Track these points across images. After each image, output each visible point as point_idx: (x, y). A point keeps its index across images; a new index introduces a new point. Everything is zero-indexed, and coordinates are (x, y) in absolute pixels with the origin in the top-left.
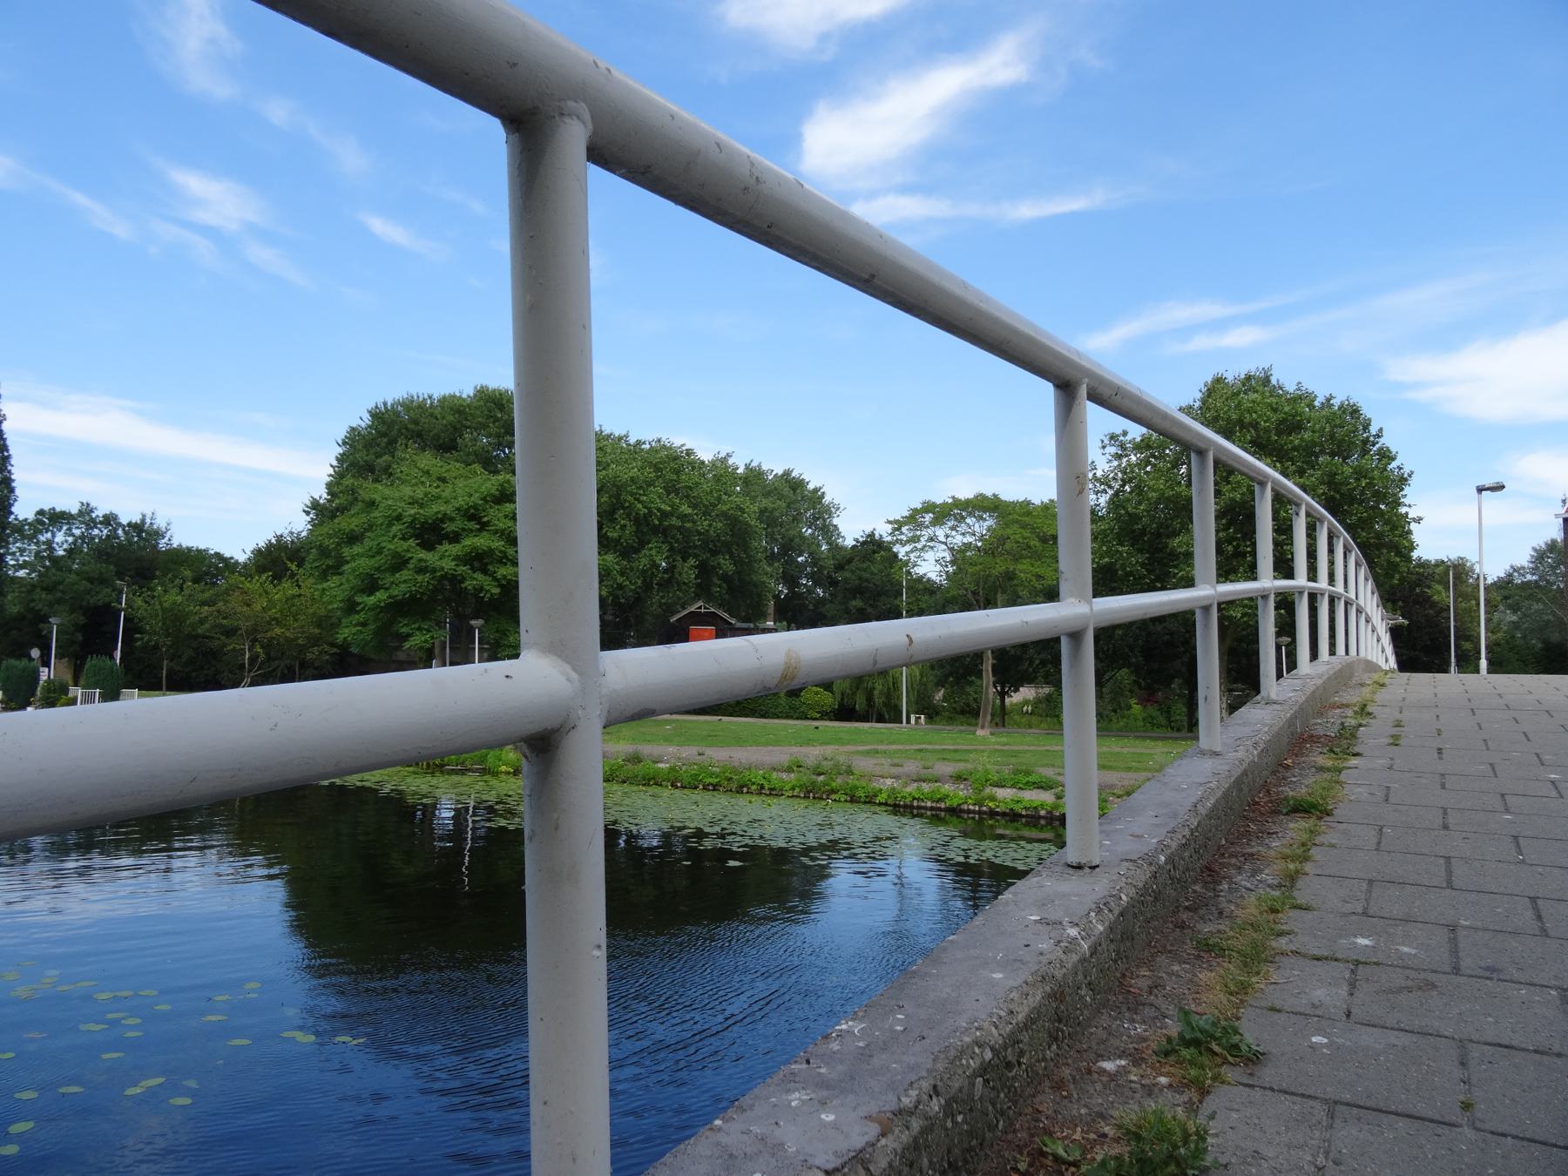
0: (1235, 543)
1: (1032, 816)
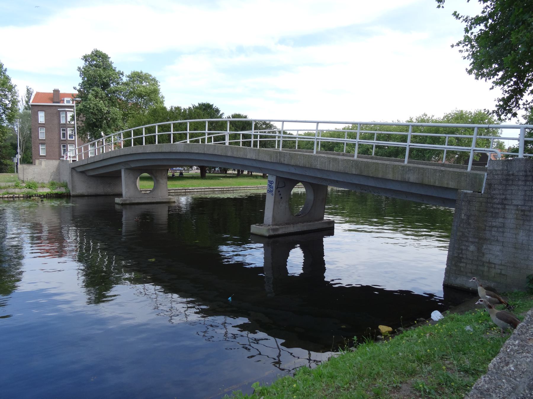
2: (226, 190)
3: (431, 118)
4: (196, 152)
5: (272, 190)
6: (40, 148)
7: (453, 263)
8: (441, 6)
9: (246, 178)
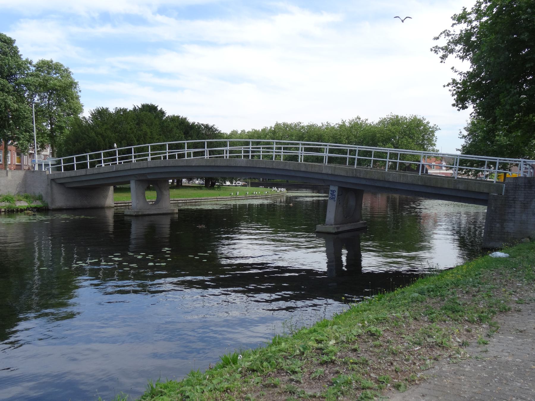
2: (188, 202)
3: (365, 122)
4: (262, 167)
5: (334, 197)
7: (487, 235)
8: (443, 62)
9: (189, 189)
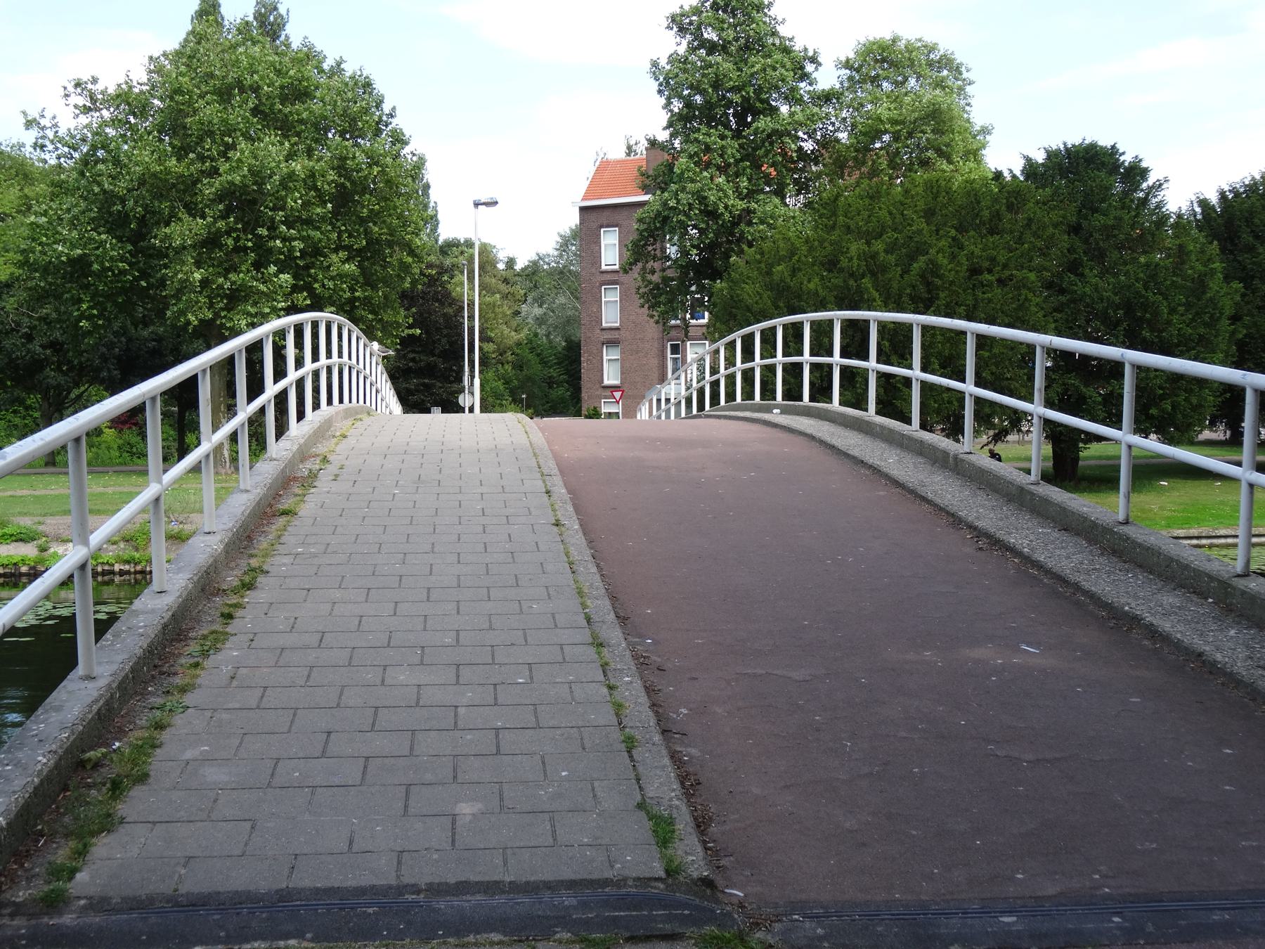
0: (235, 235)
1: (12, 575)
6: (605, 358)
